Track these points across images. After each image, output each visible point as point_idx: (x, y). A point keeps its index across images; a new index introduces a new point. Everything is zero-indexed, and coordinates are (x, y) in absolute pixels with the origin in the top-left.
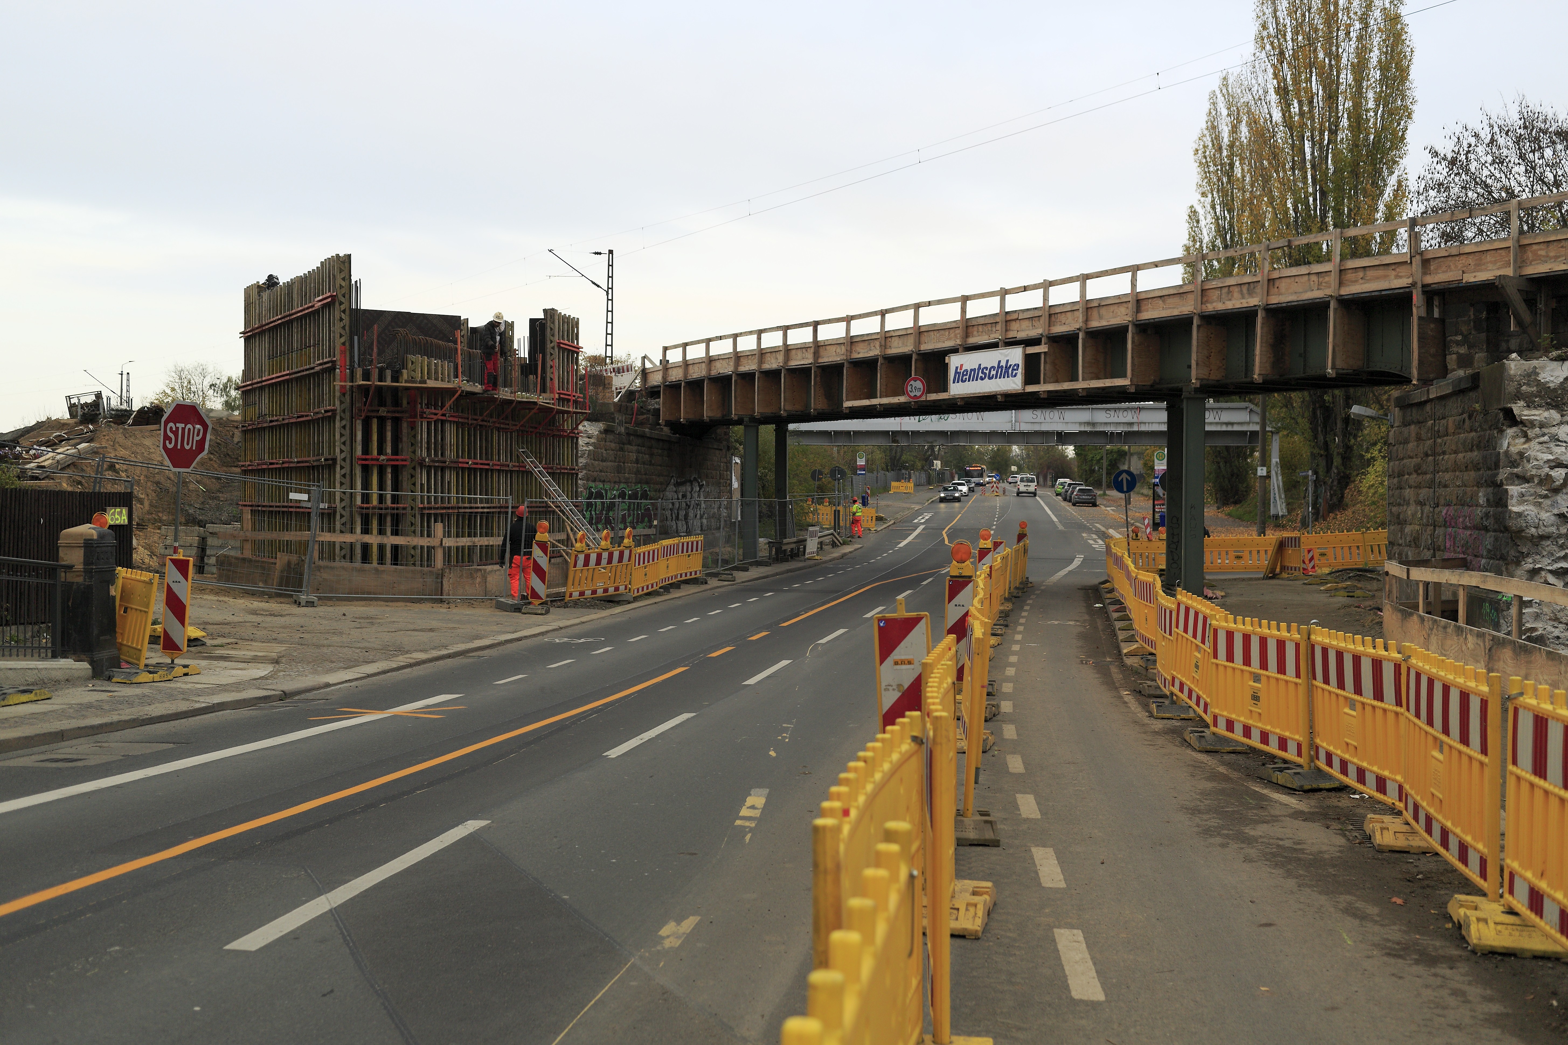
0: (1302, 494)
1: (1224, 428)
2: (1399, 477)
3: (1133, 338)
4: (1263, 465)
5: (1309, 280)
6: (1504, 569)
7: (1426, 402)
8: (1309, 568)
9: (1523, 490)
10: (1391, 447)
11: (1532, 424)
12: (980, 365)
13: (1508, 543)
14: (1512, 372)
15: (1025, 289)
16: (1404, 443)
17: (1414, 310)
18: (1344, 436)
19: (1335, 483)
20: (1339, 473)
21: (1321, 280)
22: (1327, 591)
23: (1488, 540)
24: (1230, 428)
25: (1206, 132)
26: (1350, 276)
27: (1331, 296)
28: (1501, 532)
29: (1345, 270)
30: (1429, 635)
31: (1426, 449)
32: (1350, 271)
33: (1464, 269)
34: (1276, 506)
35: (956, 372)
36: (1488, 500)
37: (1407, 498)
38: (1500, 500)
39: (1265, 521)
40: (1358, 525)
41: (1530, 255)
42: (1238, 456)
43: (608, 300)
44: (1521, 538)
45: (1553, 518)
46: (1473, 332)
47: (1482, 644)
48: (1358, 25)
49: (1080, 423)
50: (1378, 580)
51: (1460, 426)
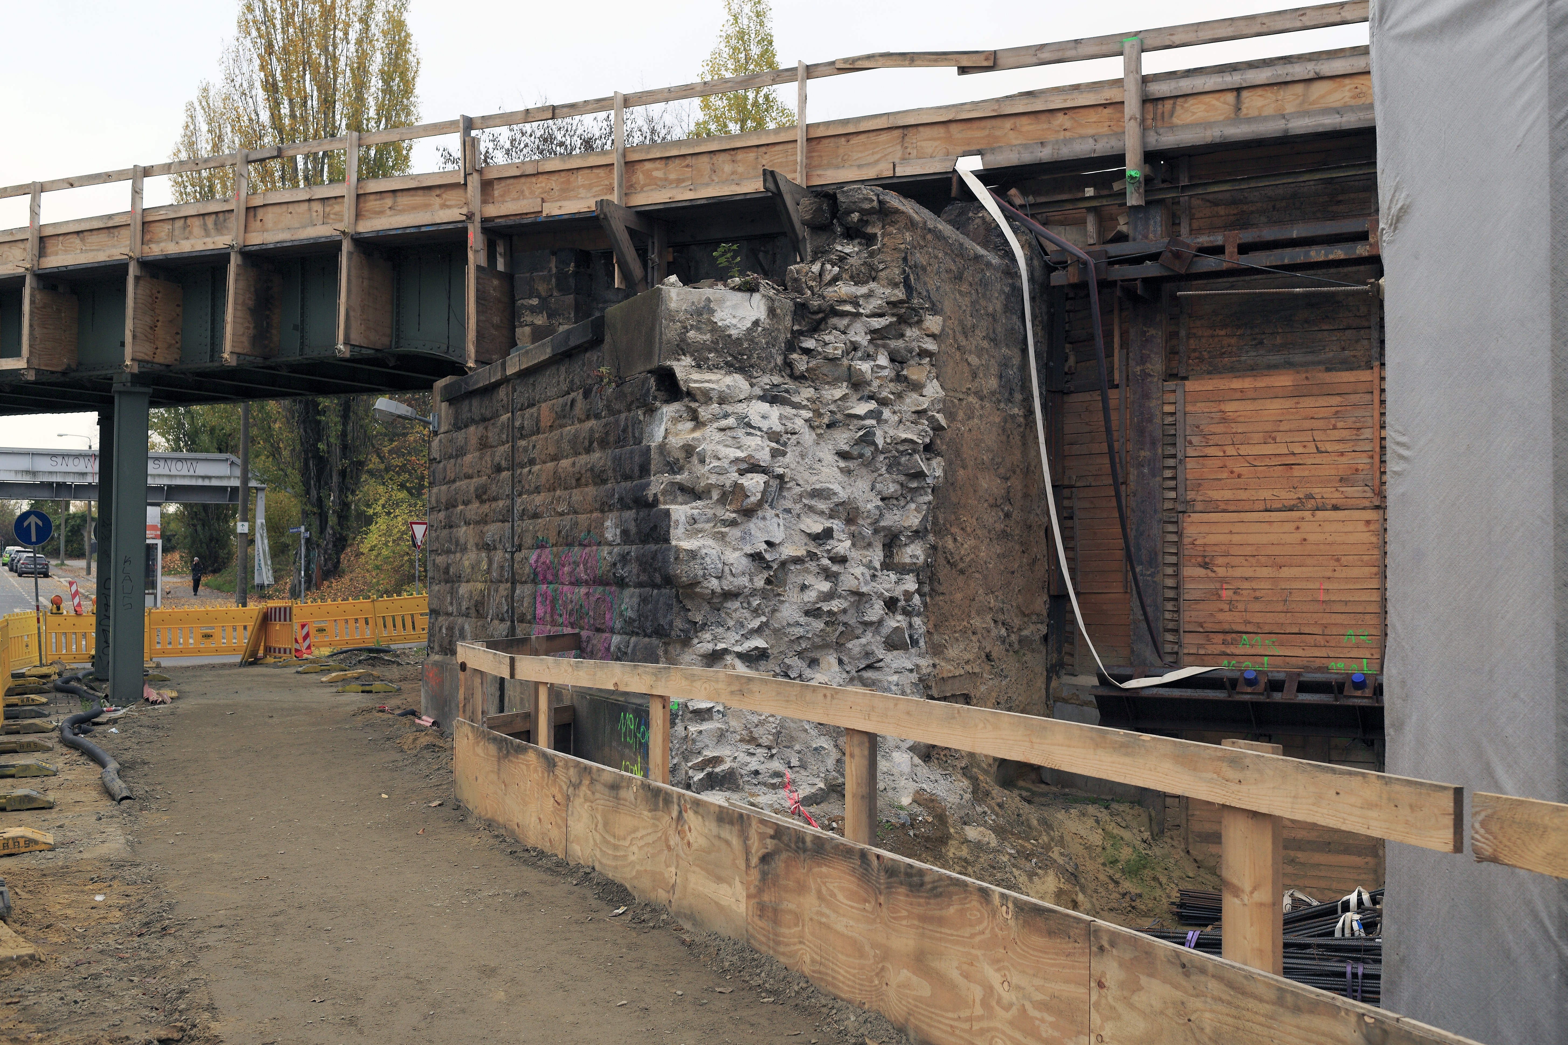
0: (292, 559)
1: (200, 482)
2: (447, 509)
3: (32, 295)
4: (244, 519)
5: (310, 210)
6: (661, 652)
7: (496, 386)
8: (304, 649)
9: (695, 512)
10: (434, 465)
11: (706, 397)
13: (670, 607)
14: (673, 305)
16: (457, 456)
17: (471, 255)
18: (341, 491)
19: (330, 546)
20: (334, 534)
21: (328, 209)
22: (332, 682)
23: (628, 601)
24: (206, 483)
25: (181, 147)
26: (372, 204)
27: (344, 233)
28: (654, 586)
29: (365, 194)
30: (568, 798)
31: (497, 459)
32: (372, 197)
33: (544, 196)
34: (260, 574)
36: (625, 533)
37: (462, 541)
38: (653, 530)
39: (247, 590)
40: (357, 594)
41: (641, 177)
42: (218, 519)
44: (693, 596)
45: (745, 561)
46: (555, 294)
47: (735, 842)
48: (358, 26)
49: (17, 472)
50: (399, 664)
51: (563, 416)
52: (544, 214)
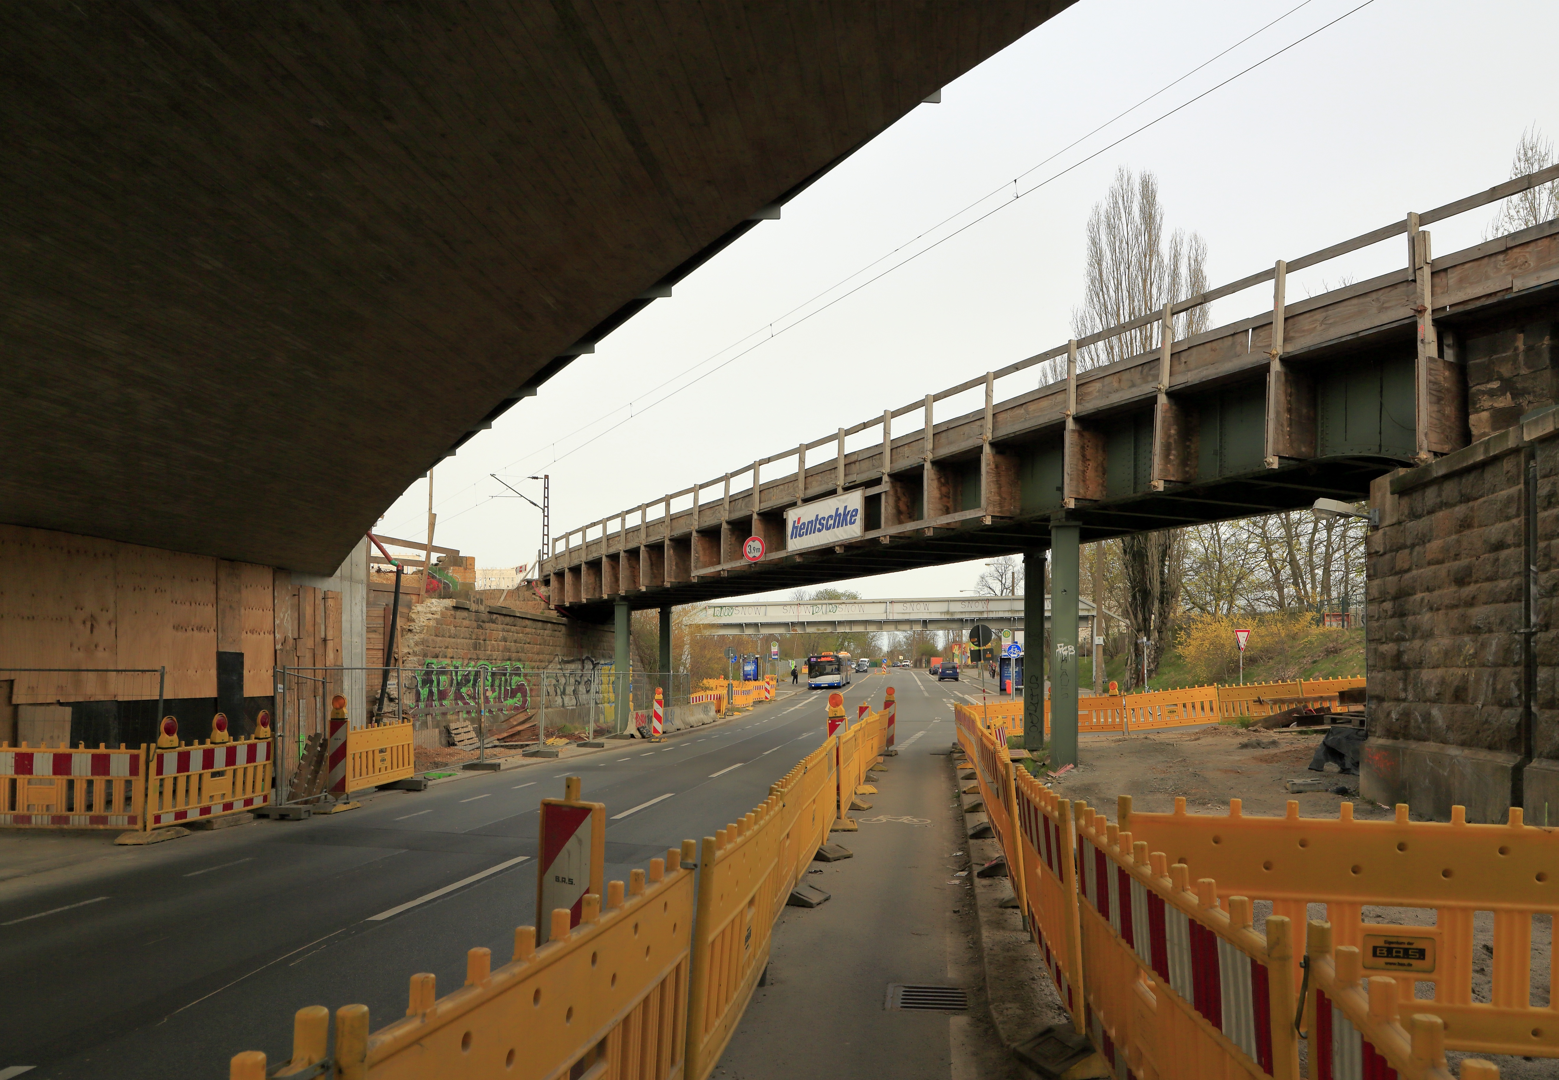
12: (817, 516)
15: (865, 426)
35: (794, 527)
43: (544, 516)
49: (941, 613)
52: (1515, 289)
